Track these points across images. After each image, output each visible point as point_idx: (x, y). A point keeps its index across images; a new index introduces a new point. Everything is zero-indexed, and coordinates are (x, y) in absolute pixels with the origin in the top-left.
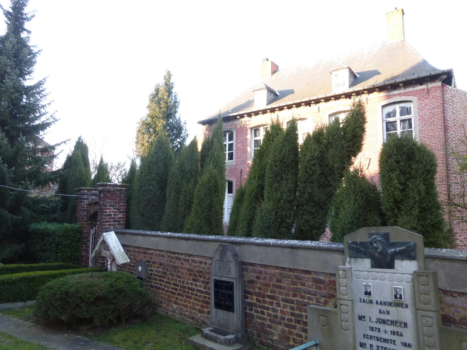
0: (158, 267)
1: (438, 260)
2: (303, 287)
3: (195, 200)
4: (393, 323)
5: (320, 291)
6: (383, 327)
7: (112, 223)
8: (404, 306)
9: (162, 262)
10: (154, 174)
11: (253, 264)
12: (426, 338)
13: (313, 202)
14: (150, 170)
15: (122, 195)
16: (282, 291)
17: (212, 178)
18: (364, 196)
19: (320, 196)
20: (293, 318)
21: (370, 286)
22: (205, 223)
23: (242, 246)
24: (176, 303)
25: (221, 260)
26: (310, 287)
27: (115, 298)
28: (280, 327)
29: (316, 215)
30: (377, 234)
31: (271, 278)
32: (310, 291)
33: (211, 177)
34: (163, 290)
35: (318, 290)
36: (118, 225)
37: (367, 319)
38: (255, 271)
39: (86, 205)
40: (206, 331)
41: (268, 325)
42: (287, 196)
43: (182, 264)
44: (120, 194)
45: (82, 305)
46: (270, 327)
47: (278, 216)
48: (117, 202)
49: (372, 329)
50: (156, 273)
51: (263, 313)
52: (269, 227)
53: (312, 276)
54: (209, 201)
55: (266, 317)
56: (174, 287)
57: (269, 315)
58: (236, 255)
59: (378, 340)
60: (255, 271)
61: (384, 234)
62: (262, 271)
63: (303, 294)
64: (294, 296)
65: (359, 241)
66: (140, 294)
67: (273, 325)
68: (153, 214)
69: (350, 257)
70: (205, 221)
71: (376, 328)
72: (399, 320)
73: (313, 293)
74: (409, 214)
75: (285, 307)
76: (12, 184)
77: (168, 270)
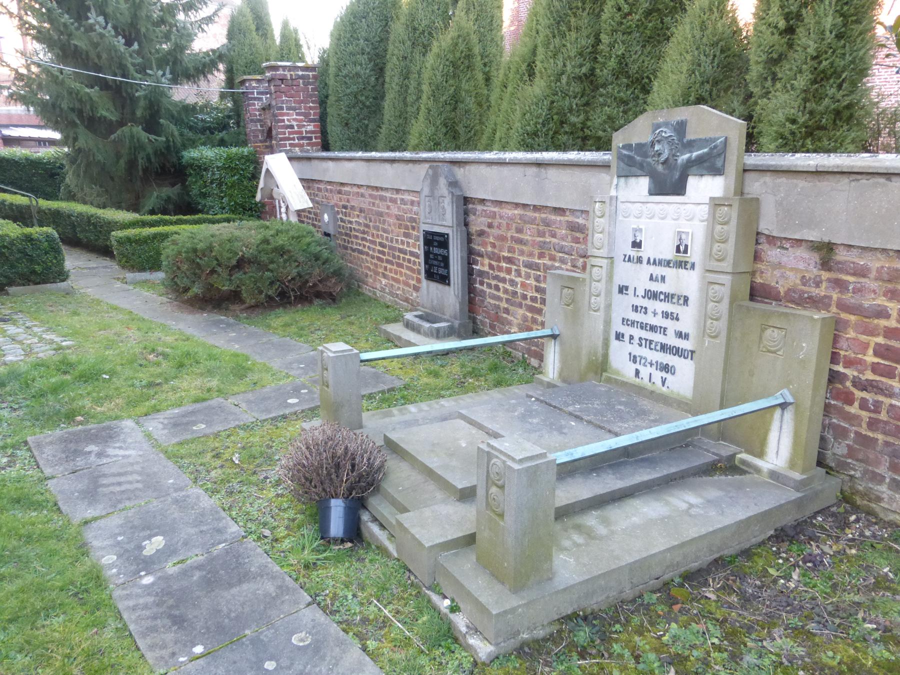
0: (358, 216)
1: (769, 174)
2: (554, 240)
3: (425, 88)
4: (669, 297)
5: (577, 245)
6: (651, 305)
7: (297, 141)
8: (689, 266)
9: (363, 206)
10: (362, 41)
11: (482, 201)
12: (710, 321)
13: (628, 77)
14: (355, 32)
15: (310, 87)
16: (524, 248)
17: (460, 40)
18: (718, 53)
19: (643, 62)
20: (539, 296)
21: (640, 230)
22: (445, 134)
23: (467, 167)
24: (385, 276)
25: (432, 195)
26: (562, 239)
27: (272, 262)
28: (521, 312)
29: (631, 105)
30: (666, 124)
31: (508, 224)
32: (562, 247)
33: (459, 36)
34: (368, 254)
35: (574, 245)
36: (308, 145)
37: (631, 291)
38: (485, 214)
39: (259, 110)
40: (409, 316)
41: (505, 308)
42: (574, 67)
43: (388, 208)
44: (306, 84)
45: (219, 270)
46: (507, 311)
47: (555, 111)
48: (302, 102)
49: (636, 309)
50: (357, 227)
51: (497, 288)
52: (535, 134)
53: (566, 218)
54: (453, 89)
55: (502, 295)
56: (381, 249)
57: (506, 291)
58: (454, 184)
59: (642, 328)
60: (485, 214)
61: (678, 123)
62: (495, 212)
63: (553, 253)
64: (541, 256)
65: (634, 141)
66: (317, 257)
67: (511, 308)
68: (366, 122)
69: (619, 177)
70: (444, 130)
71: (642, 307)
72: (678, 293)
73: (566, 250)
74: (789, 88)
75: (528, 276)
76: (139, 76)
77: (371, 221)
